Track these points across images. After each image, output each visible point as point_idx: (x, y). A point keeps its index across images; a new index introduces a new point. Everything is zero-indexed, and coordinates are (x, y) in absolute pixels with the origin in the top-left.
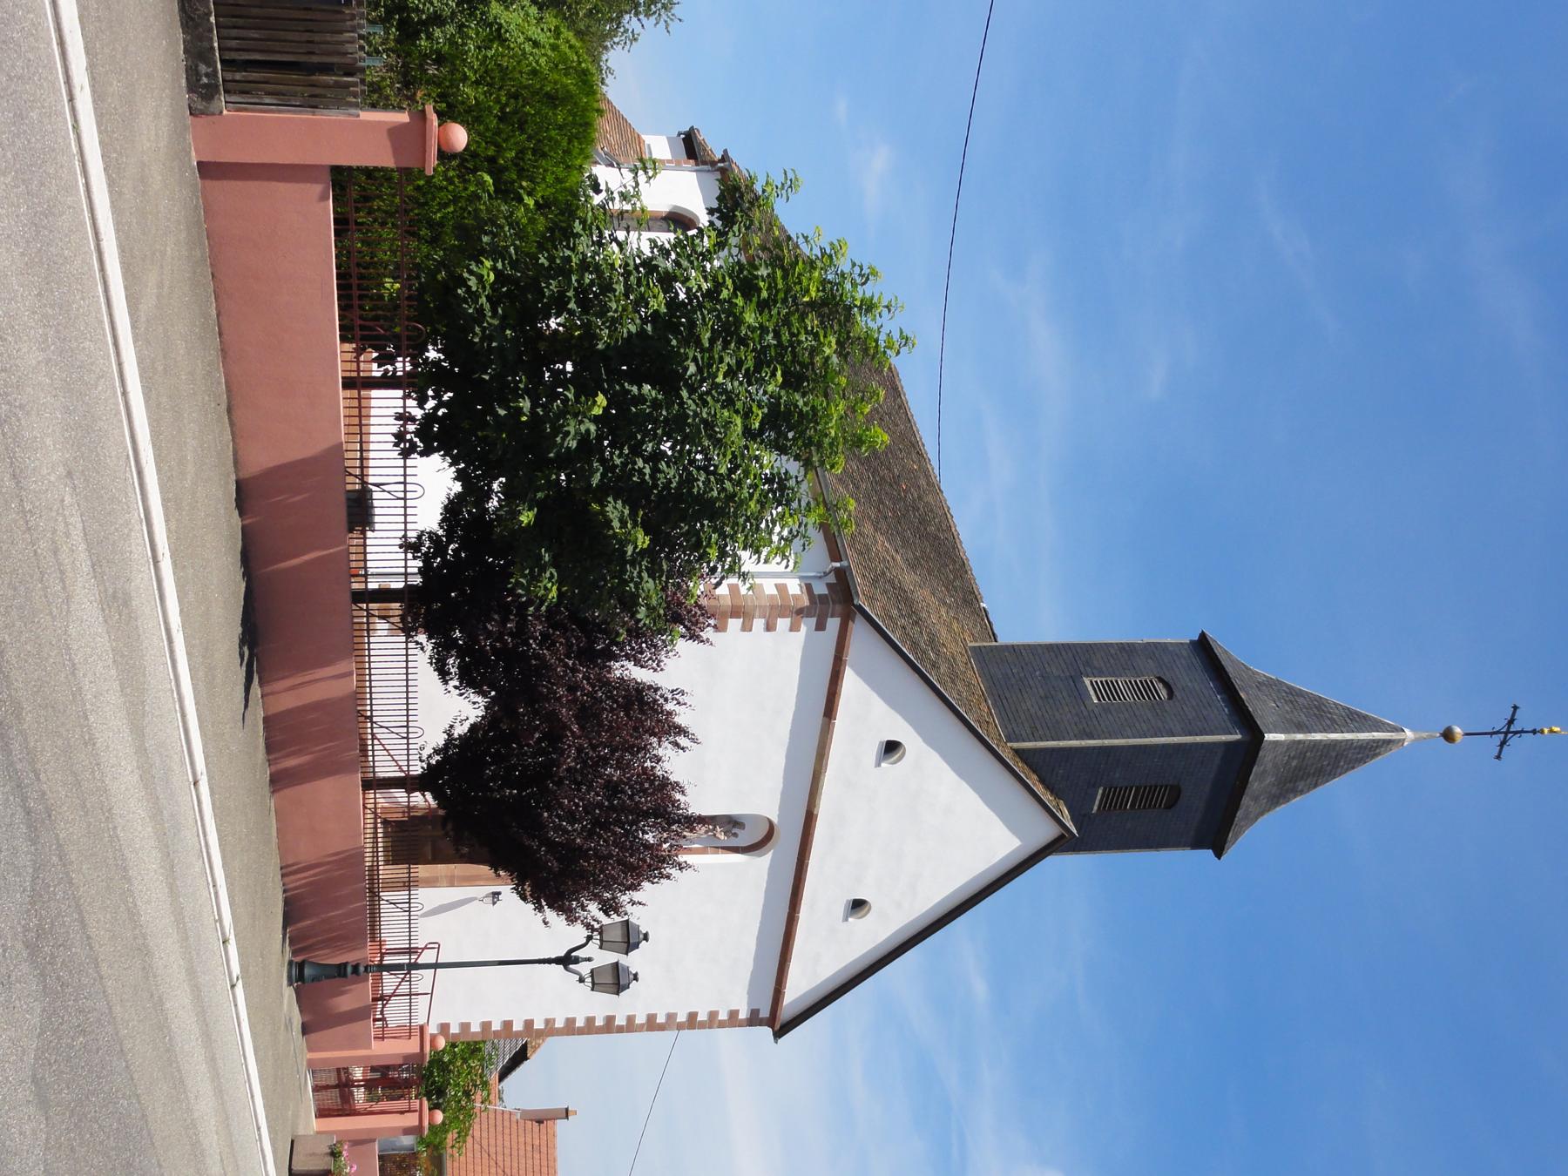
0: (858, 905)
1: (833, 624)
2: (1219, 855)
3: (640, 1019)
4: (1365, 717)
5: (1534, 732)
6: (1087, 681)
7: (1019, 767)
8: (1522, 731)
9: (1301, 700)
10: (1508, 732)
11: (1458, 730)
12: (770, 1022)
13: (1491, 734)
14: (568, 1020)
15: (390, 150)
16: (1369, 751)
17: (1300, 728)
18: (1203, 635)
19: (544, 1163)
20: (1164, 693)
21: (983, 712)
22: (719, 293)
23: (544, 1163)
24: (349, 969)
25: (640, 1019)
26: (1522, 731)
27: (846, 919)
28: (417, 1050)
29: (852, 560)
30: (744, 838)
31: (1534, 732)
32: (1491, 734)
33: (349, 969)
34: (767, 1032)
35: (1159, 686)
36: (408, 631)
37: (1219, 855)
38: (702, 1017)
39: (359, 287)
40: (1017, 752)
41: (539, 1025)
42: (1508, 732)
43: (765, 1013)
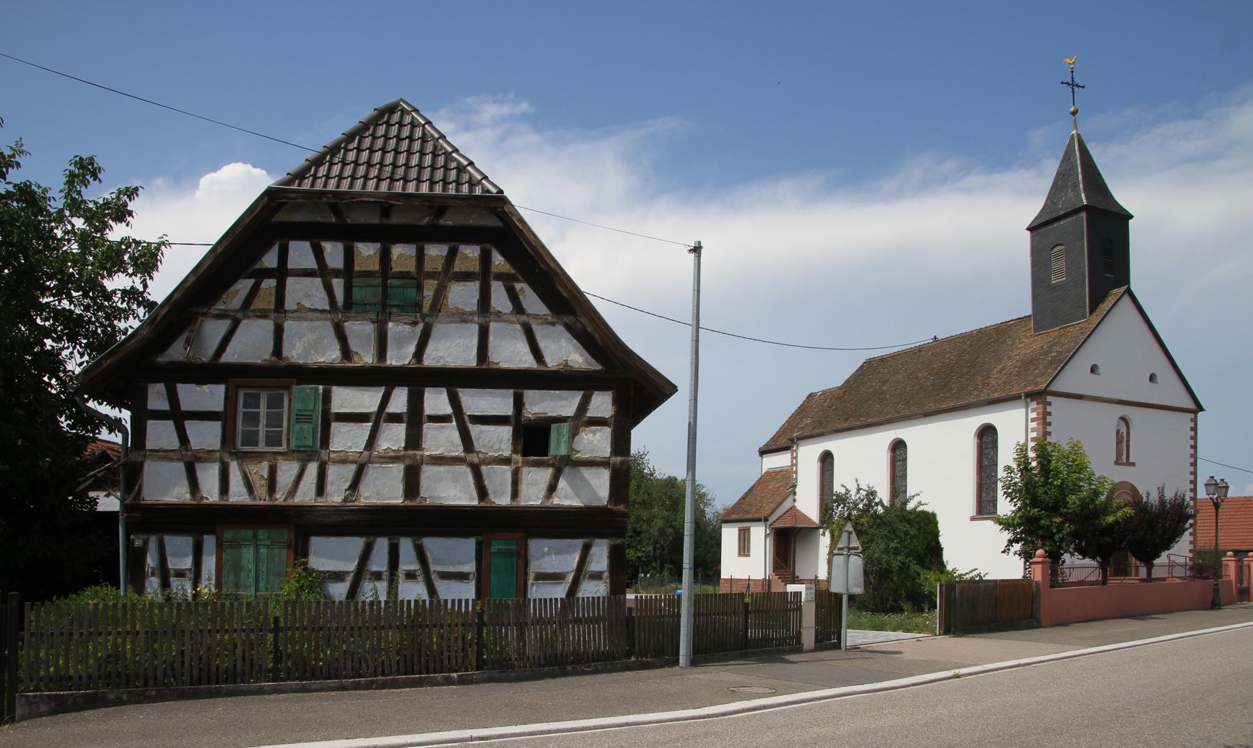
0: (1152, 378)
1: (1049, 399)
2: (1131, 217)
4: (1066, 153)
7: (1104, 307)
10: (1073, 85)
12: (1195, 412)
15: (462, 540)
17: (1076, 185)
18: (740, 555)
21: (1075, 329)
25: (1192, 469)
28: (1040, 566)
29: (1022, 392)
30: (1124, 430)
34: (1200, 414)
36: (66, 597)
37: (1131, 217)
40: (1091, 312)
42: (1073, 85)
43: (1192, 416)
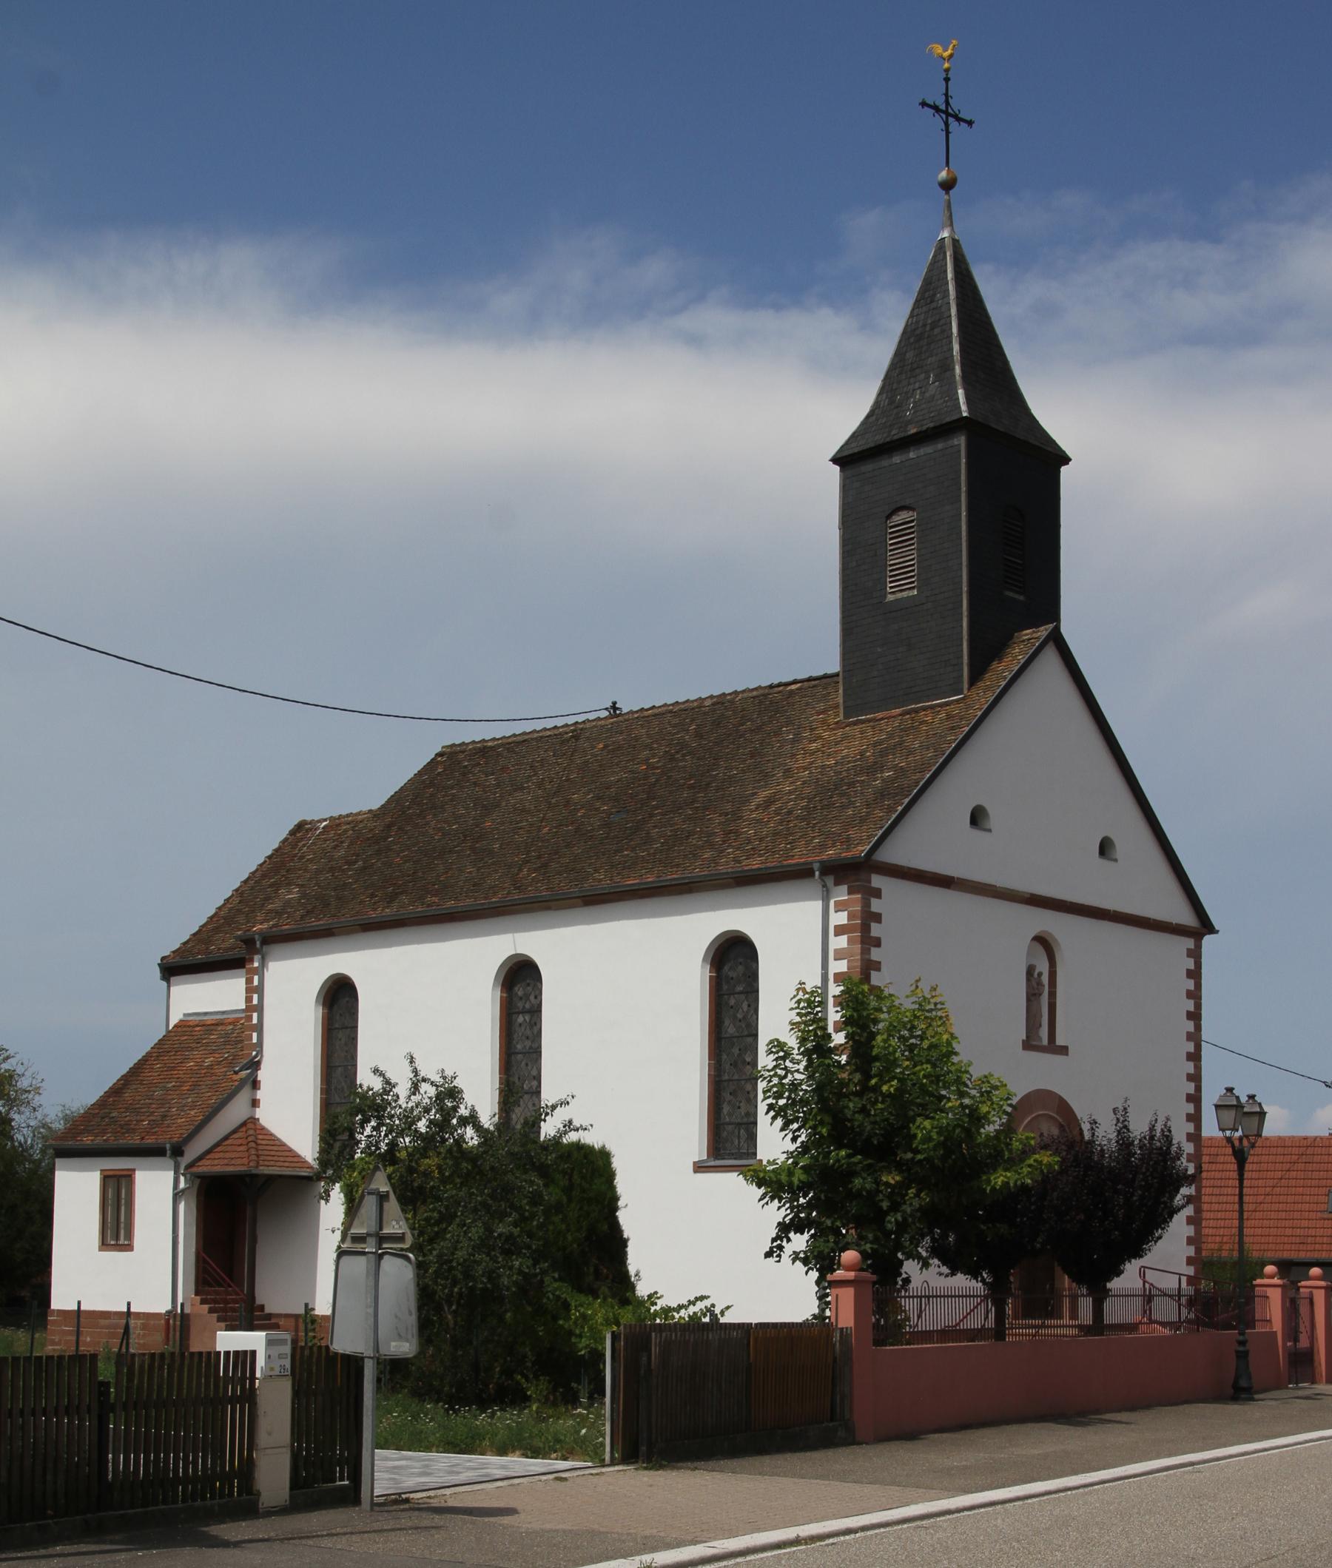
0: (1105, 848)
3: (1190, 1067)
5: (947, 80)
6: (890, 598)
8: (946, 95)
9: (910, 355)
10: (947, 113)
11: (943, 175)
13: (948, 133)
14: (1188, 1223)
16: (956, 243)
17: (946, 367)
19: (1280, 1150)
20: (904, 516)
22: (881, 1208)
23: (1280, 1150)
24: (1241, 1349)
26: (946, 95)
27: (1116, 860)
30: (1043, 967)
31: (947, 80)
32: (948, 133)
33: (1241, 1349)
34: (1208, 940)
35: (898, 518)
38: (1191, 1088)
39: (194, 1500)
41: (1191, 1251)
42: (947, 113)
43: (1190, 943)
